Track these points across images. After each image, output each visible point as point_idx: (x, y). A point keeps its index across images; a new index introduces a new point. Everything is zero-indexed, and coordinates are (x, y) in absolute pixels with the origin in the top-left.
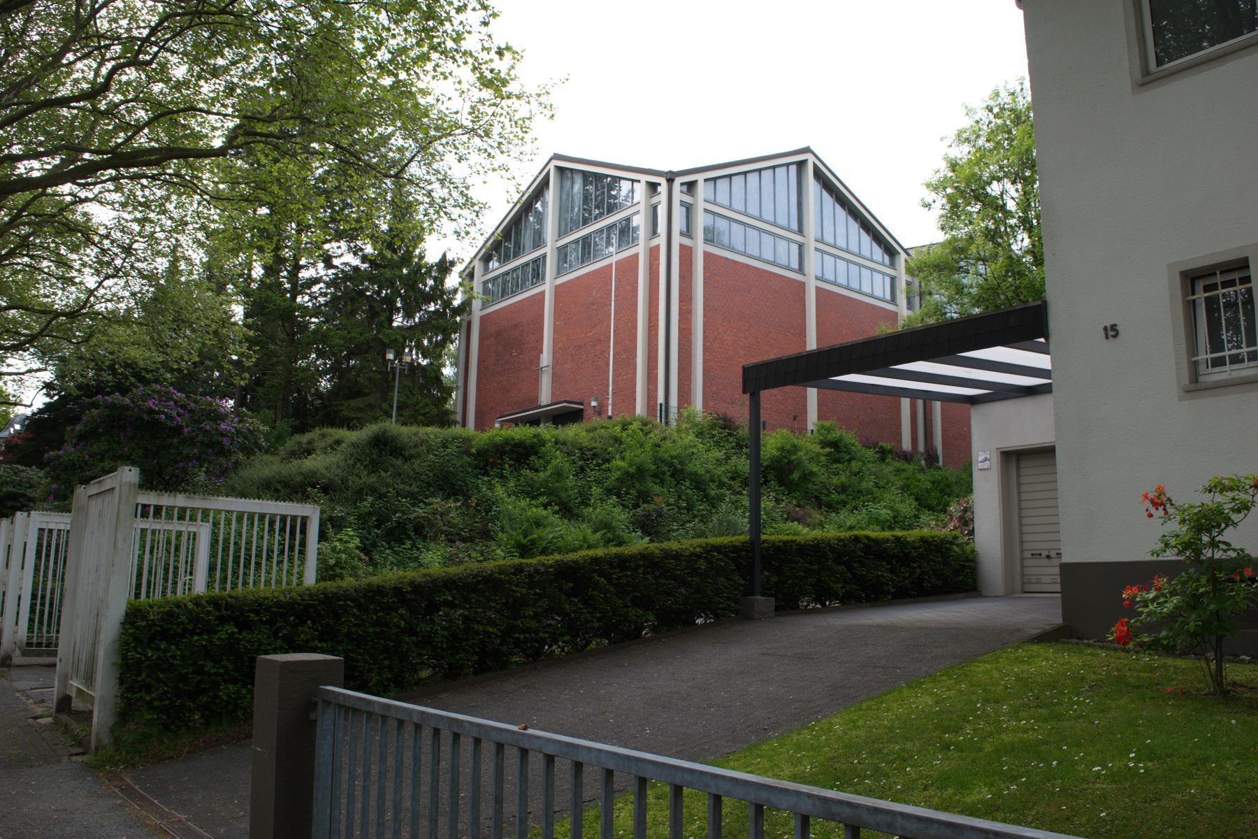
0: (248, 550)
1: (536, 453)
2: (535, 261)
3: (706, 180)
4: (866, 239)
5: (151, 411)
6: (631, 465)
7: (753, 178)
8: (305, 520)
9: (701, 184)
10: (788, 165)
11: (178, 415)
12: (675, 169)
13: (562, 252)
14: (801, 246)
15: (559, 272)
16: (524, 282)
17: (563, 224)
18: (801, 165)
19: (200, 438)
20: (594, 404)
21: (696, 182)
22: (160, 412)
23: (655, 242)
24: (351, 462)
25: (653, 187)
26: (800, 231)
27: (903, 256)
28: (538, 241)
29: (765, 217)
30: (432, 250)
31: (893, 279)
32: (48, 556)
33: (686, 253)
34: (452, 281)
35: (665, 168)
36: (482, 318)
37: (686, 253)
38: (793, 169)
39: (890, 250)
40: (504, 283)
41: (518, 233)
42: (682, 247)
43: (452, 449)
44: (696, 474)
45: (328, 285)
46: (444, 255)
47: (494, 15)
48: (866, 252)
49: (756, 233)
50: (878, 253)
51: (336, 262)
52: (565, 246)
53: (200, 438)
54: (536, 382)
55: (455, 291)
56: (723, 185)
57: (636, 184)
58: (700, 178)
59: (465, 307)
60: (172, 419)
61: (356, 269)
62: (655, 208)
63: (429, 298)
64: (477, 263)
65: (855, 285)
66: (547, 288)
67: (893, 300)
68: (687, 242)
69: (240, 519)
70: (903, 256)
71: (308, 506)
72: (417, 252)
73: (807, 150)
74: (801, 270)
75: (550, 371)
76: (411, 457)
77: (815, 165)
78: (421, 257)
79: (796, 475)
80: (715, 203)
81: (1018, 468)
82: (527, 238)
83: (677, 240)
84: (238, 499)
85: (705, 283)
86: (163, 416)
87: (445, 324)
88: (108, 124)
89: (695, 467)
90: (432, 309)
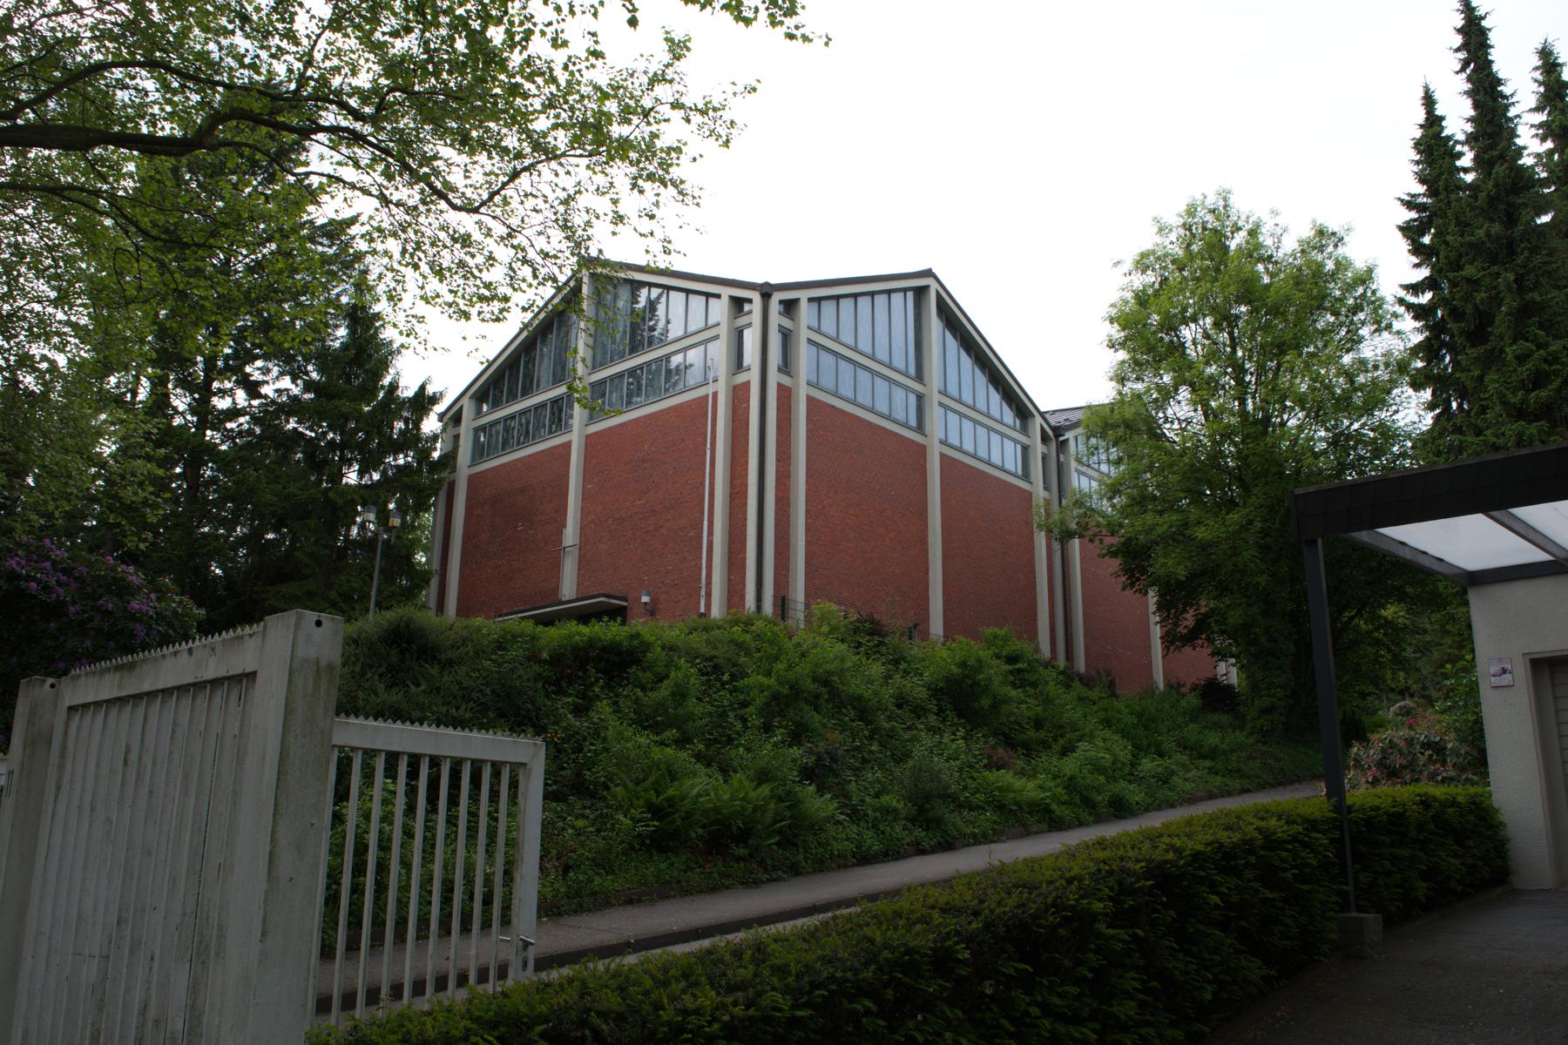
1: (638, 662)
3: (810, 300)
4: (995, 397)
6: (780, 683)
7: (864, 303)
8: (517, 767)
9: (804, 304)
10: (905, 290)
11: (59, 584)
12: (772, 282)
14: (920, 398)
16: (537, 429)
17: (599, 351)
18: (920, 292)
19: (95, 623)
20: (645, 599)
21: (797, 300)
22: (29, 578)
23: (741, 378)
24: (358, 668)
25: (738, 304)
26: (919, 377)
27: (1038, 420)
28: (561, 373)
29: (879, 356)
30: (407, 373)
31: (1025, 449)
33: (785, 394)
34: (430, 425)
35: (759, 279)
37: (785, 394)
38: (910, 295)
39: (1020, 405)
40: (507, 430)
41: (530, 361)
42: (780, 386)
43: (516, 652)
44: (860, 698)
45: (255, 420)
46: (423, 388)
47: (595, 15)
48: (995, 412)
49: (868, 375)
50: (1009, 416)
51: (267, 390)
52: (602, 382)
53: (95, 623)
54: (557, 566)
55: (435, 438)
56: (828, 308)
57: (712, 301)
58: (803, 295)
59: (449, 459)
60: (46, 588)
61: (295, 399)
62: (739, 334)
63: (398, 448)
64: (466, 401)
65: (982, 453)
67: (1026, 475)
68: (786, 380)
70: (1038, 420)
71: (522, 740)
72: (386, 381)
73: (928, 273)
74: (920, 428)
76: (450, 663)
77: (938, 293)
78: (393, 387)
79: (985, 702)
80: (818, 331)
81: (1554, 685)
82: (544, 368)
83: (774, 377)
84: (389, 724)
85: (808, 438)
86: (34, 585)
87: (425, 482)
89: (855, 686)
90: (401, 462)
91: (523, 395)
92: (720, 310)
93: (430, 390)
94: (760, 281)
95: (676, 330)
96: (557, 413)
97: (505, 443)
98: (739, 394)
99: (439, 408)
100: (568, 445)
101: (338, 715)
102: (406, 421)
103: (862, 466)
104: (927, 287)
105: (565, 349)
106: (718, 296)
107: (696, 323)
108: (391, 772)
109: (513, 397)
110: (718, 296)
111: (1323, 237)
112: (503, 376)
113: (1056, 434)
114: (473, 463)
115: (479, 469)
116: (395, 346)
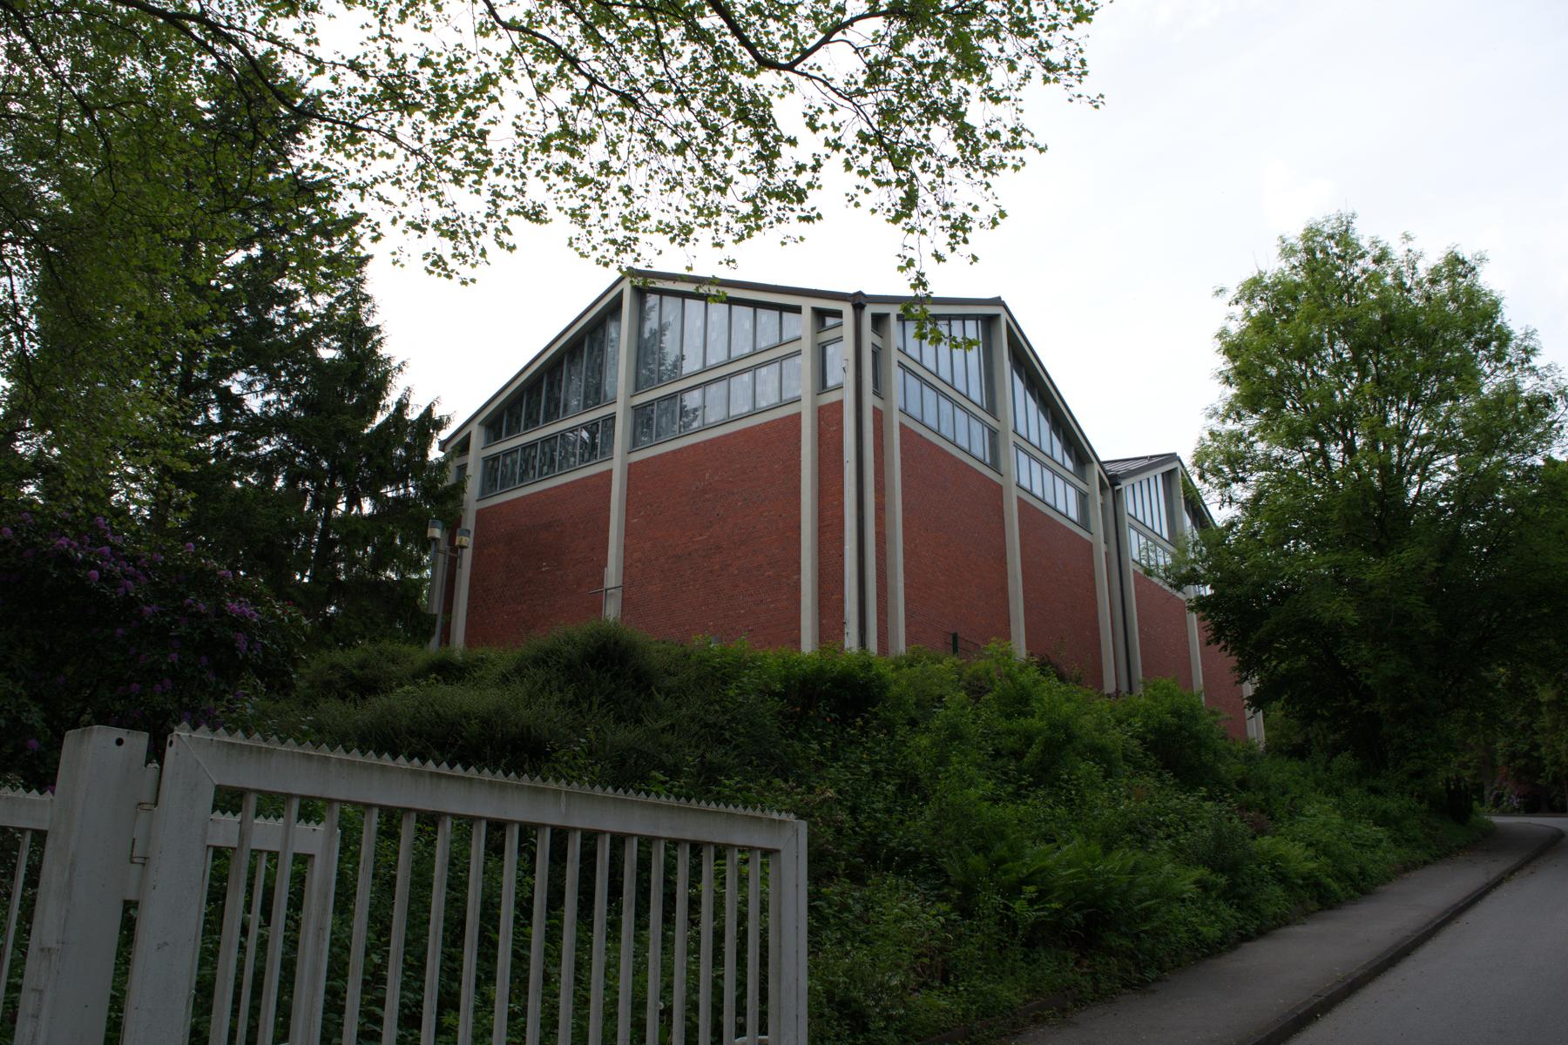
0: (614, 926)
2: (592, 427)
5: (64, 560)
8: (303, 860)
12: (867, 292)
13: (491, 463)
15: (635, 444)
16: (524, 473)
21: (887, 315)
26: (992, 409)
28: (596, 395)
32: (615, 891)
36: (480, 513)
41: (554, 385)
46: (429, 410)
53: (183, 629)
66: (617, 464)
67: (1084, 522)
69: (389, 832)
70: (1097, 467)
73: (998, 302)
74: (995, 465)
75: (619, 593)
83: (869, 400)
88: (36, 111)
91: (508, 434)
92: (799, 326)
93: (436, 414)
94: (852, 291)
95: (691, 364)
96: (597, 442)
97: (524, 473)
98: (828, 417)
99: (444, 434)
100: (608, 474)
101: (214, 809)
102: (407, 447)
103: (952, 501)
104: (998, 316)
105: (598, 370)
106: (797, 310)
107: (742, 346)
108: (495, 849)
109: (533, 423)
110: (797, 310)
111: (1455, 265)
112: (520, 400)
113: (1113, 481)
114: (485, 492)
115: (637, 457)
116: (395, 364)
